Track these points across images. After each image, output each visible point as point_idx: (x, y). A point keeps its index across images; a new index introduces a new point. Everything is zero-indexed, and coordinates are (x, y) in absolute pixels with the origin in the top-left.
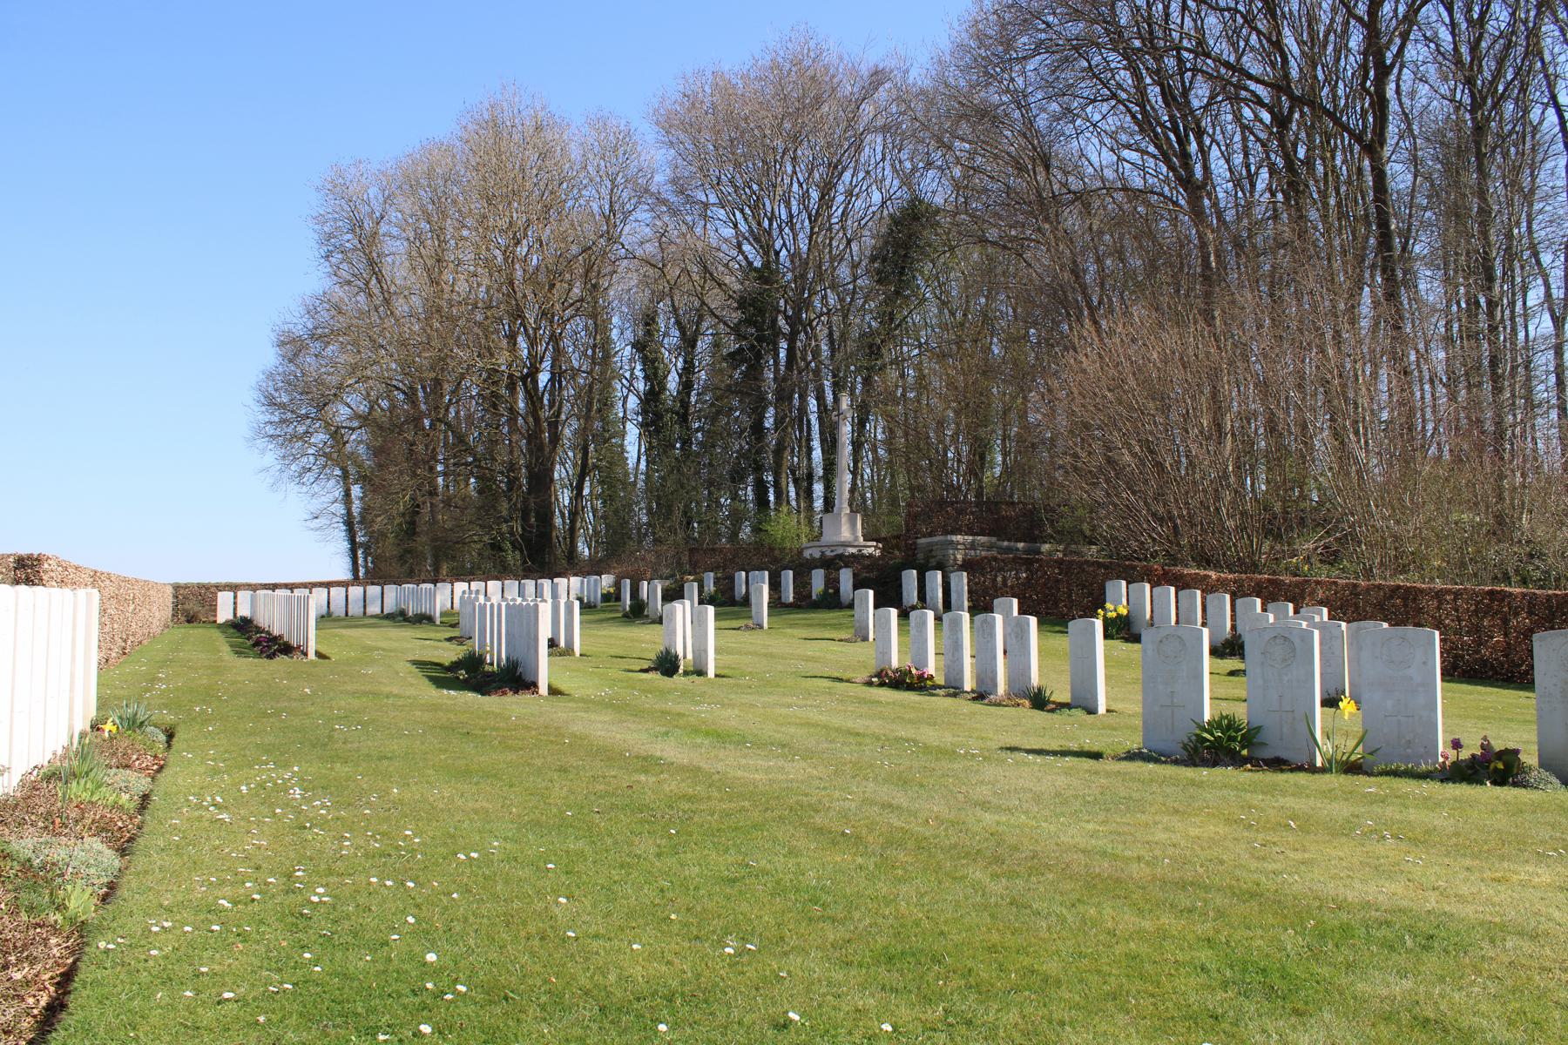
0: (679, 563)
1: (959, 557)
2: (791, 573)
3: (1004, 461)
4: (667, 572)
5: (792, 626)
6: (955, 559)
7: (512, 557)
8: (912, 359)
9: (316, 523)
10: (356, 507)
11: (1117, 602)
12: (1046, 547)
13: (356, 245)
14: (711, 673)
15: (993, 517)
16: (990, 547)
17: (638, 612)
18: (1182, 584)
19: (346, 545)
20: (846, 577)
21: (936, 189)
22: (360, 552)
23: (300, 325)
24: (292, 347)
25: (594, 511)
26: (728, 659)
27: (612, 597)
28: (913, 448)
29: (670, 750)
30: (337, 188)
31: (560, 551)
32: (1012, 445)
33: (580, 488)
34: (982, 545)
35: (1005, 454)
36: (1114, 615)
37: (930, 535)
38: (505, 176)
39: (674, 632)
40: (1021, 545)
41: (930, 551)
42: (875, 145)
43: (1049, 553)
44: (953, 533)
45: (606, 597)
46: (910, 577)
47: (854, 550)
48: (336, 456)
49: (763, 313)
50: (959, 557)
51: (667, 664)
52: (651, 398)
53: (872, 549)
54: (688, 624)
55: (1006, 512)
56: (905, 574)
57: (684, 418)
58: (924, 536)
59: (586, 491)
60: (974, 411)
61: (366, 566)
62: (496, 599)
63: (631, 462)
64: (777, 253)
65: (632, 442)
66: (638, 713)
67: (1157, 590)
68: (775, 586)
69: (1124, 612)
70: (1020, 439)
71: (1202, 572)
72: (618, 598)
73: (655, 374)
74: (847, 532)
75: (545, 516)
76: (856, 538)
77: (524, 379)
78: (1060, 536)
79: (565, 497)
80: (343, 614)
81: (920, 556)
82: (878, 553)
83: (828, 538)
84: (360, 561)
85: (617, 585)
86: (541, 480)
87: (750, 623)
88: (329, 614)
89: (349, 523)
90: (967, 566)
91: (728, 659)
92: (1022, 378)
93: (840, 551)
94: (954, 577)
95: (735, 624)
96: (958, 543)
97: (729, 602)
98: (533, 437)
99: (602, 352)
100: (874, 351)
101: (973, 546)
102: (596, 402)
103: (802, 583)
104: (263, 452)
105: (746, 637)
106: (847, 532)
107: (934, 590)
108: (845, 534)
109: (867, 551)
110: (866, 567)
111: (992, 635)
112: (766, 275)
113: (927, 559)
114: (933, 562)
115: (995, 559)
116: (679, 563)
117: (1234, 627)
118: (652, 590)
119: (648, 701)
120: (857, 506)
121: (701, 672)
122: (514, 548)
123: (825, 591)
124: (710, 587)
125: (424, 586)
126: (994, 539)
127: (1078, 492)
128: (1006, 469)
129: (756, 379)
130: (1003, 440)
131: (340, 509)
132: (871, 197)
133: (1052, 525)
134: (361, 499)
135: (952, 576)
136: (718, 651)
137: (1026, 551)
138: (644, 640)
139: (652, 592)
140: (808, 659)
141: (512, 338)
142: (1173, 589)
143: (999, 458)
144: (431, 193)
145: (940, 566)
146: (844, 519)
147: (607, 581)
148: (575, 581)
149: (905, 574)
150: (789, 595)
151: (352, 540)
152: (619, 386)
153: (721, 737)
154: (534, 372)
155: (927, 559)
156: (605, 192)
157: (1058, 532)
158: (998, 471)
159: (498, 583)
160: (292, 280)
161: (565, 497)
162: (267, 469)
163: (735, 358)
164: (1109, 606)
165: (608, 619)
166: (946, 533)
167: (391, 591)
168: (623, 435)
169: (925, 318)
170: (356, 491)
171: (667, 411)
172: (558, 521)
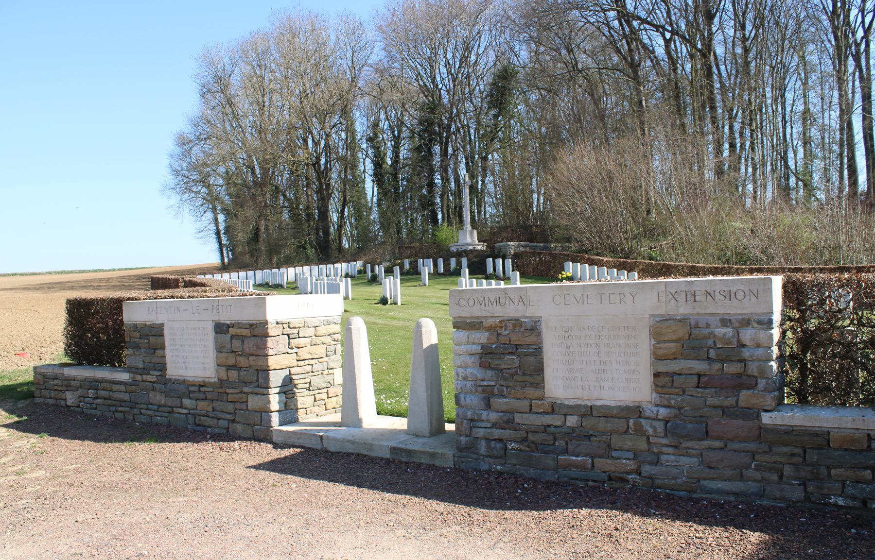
0: (394, 254)
4: (388, 258)
5: (438, 284)
7: (311, 252)
9: (201, 235)
10: (222, 226)
13: (217, 88)
14: (399, 304)
16: (526, 247)
17: (374, 280)
18: (592, 262)
19: (217, 246)
20: (464, 261)
23: (187, 129)
24: (183, 141)
25: (351, 224)
26: (408, 298)
27: (362, 272)
29: (380, 321)
31: (334, 246)
33: (342, 212)
37: (501, 242)
38: (297, 52)
39: (386, 289)
40: (542, 245)
45: (360, 272)
46: (490, 261)
47: (471, 247)
48: (212, 200)
49: (433, 126)
51: (384, 301)
52: (378, 164)
54: (392, 285)
57: (395, 177)
59: (346, 214)
61: (228, 257)
62: (308, 275)
63: (369, 199)
65: (370, 187)
66: (373, 315)
68: (435, 265)
72: (365, 272)
73: (379, 155)
75: (327, 233)
76: (474, 241)
77: (314, 165)
78: (557, 240)
79: (335, 217)
83: (460, 242)
84: (225, 254)
85: (364, 266)
86: (324, 214)
87: (421, 283)
89: (218, 233)
91: (408, 298)
93: (465, 248)
95: (415, 284)
97: (411, 274)
98: (319, 191)
99: (351, 145)
101: (518, 246)
102: (350, 165)
104: (169, 197)
105: (418, 289)
106: (470, 239)
108: (469, 240)
109: (479, 247)
110: (476, 257)
113: (499, 253)
114: (501, 254)
116: (394, 254)
118: (380, 270)
119: (376, 312)
121: (396, 304)
122: (312, 247)
123: (456, 269)
124: (407, 266)
125: (273, 270)
131: (213, 227)
132: (486, 61)
134: (225, 221)
136: (402, 295)
138: (375, 291)
139: (380, 271)
140: (438, 297)
141: (305, 141)
147: (359, 264)
148: (344, 265)
150: (441, 270)
151: (220, 243)
152: (360, 155)
153: (394, 318)
154: (318, 159)
155: (499, 253)
156: (349, 55)
159: (308, 267)
160: (180, 107)
161: (335, 217)
162: (172, 206)
163: (418, 149)
167: (259, 273)
168: (364, 182)
170: (221, 218)
171: (386, 173)
172: (332, 229)
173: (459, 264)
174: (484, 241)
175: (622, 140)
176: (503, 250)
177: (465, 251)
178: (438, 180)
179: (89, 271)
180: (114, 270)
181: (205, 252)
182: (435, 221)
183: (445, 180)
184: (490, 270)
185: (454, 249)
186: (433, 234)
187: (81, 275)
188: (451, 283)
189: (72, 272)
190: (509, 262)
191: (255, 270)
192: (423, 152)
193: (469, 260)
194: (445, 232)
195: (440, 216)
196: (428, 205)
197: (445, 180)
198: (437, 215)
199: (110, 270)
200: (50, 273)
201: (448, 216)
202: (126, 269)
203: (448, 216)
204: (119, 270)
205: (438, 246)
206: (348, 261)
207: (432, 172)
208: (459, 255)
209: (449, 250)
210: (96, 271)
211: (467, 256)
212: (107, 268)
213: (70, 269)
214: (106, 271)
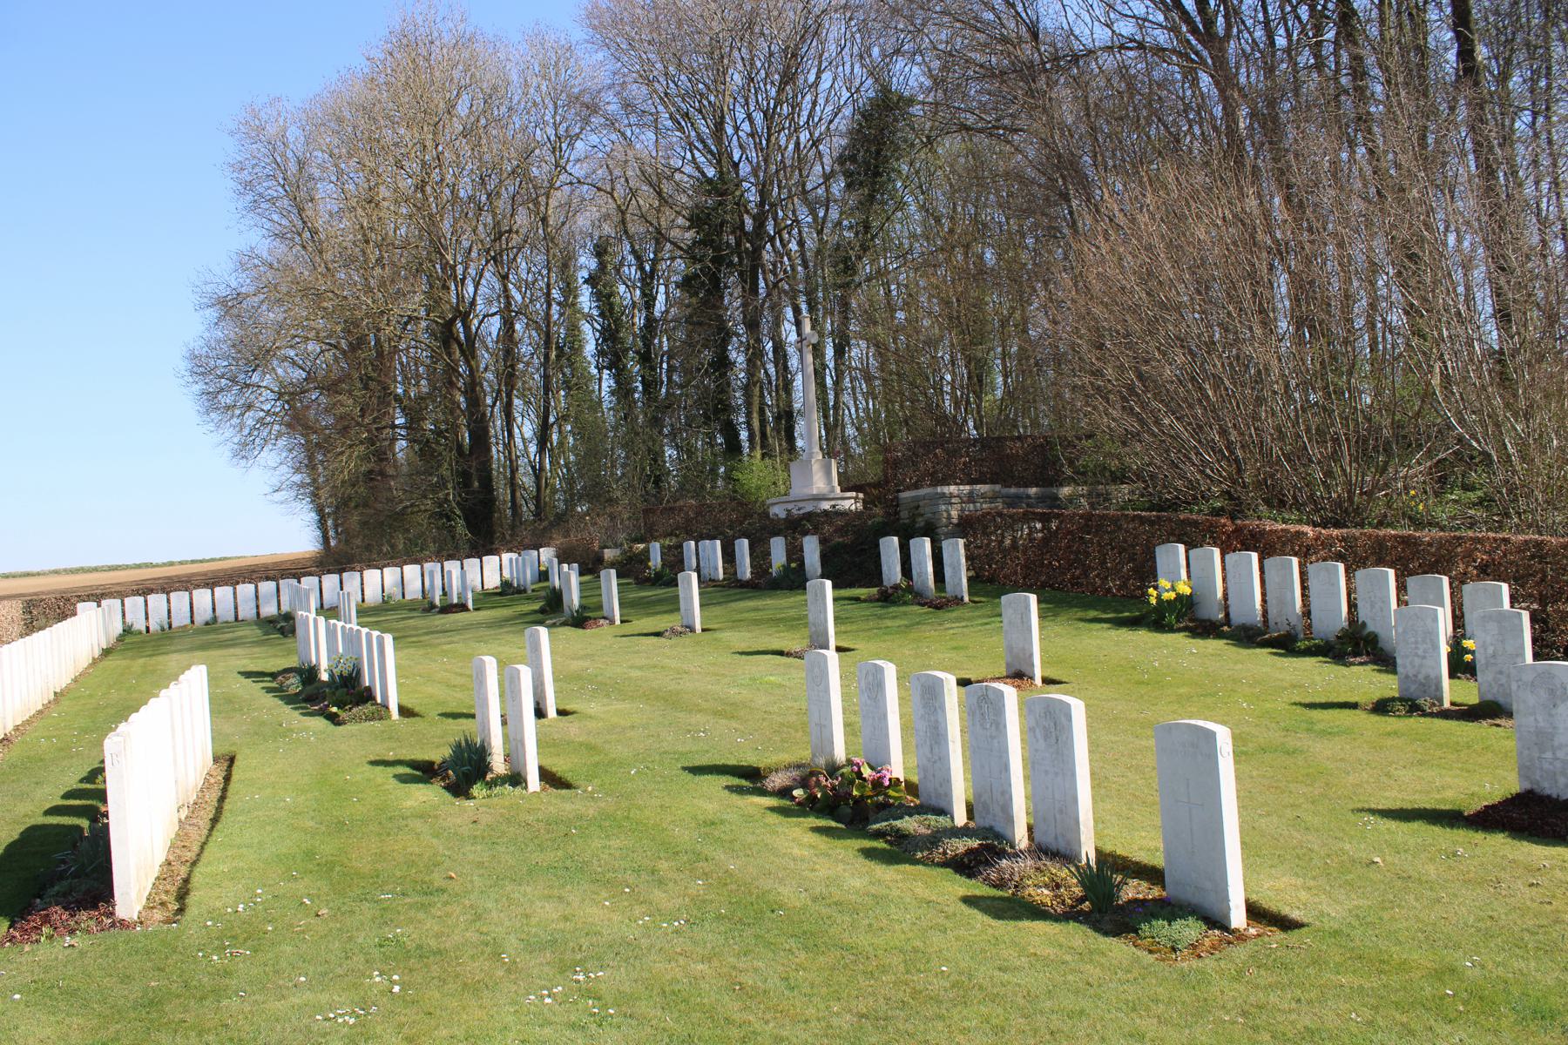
1: (954, 513)
2: (746, 541)
3: (1005, 382)
5: (736, 624)
6: (949, 517)
8: (903, 280)
11: (1174, 579)
12: (1066, 491)
13: (284, 187)
15: (998, 459)
16: (993, 498)
18: (1268, 547)
19: (313, 516)
20: (811, 549)
21: (910, 77)
22: (330, 522)
24: (229, 306)
28: (902, 376)
30: (253, 130)
32: (1012, 364)
34: (983, 496)
35: (1006, 376)
36: (1172, 595)
37: (916, 486)
38: (417, 98)
40: (1033, 491)
41: (915, 507)
42: (834, 30)
43: (1070, 499)
44: (945, 481)
46: (890, 546)
47: (826, 506)
49: (723, 241)
50: (954, 513)
52: (610, 336)
53: (850, 503)
55: (1015, 448)
56: (883, 542)
58: (908, 488)
60: (970, 331)
64: (736, 165)
67: (1231, 558)
68: (729, 556)
69: (1188, 591)
70: (1023, 355)
71: (1293, 528)
73: (611, 309)
74: (818, 482)
76: (832, 490)
78: (1080, 476)
80: (232, 618)
81: (904, 514)
82: (860, 506)
83: (798, 491)
88: (215, 619)
90: (965, 527)
92: (1019, 282)
93: (809, 508)
94: (946, 545)
96: (952, 496)
100: (847, 267)
101: (971, 498)
103: (760, 556)
106: (818, 482)
107: (922, 564)
108: (819, 484)
110: (839, 530)
111: (999, 725)
112: (721, 187)
113: (913, 518)
114: (920, 522)
115: (1000, 514)
117: (1352, 606)
120: (833, 445)
123: (786, 568)
126: (998, 487)
127: (1112, 418)
128: (1008, 393)
129: (714, 307)
130: (1003, 360)
132: (833, 95)
133: (1071, 463)
135: (945, 544)
137: (1041, 499)
142: (1255, 556)
143: (1000, 380)
144: (359, 129)
145: (930, 530)
146: (816, 467)
149: (883, 542)
150: (746, 571)
155: (913, 518)
157: (1077, 472)
158: (999, 393)
160: (224, 239)
164: (1164, 583)
165: (507, 620)
166: (937, 482)
169: (907, 222)
173: (795, 553)
174: (857, 488)
175: (225, 1002)
176: (927, 511)
177: (809, 516)
178: (738, 357)
179: (127, 567)
180: (171, 564)
181: (297, 534)
182: (733, 447)
183: (755, 356)
184: (892, 571)
185: (778, 511)
186: (728, 478)
187: (112, 574)
188: (775, 622)
189: (96, 569)
190: (956, 551)
191: (340, 572)
192: (703, 288)
193: (823, 542)
194: (756, 471)
195: (744, 435)
196: (717, 411)
197: (755, 356)
198: (737, 435)
199: (164, 565)
200: (56, 572)
201: (764, 435)
202: (193, 562)
203: (764, 435)
204: (181, 563)
205: (741, 504)
206: (519, 547)
207: (725, 335)
208: (795, 527)
209: (767, 515)
210: (139, 566)
211: (816, 530)
212: (160, 561)
213: (94, 565)
214: (157, 566)
